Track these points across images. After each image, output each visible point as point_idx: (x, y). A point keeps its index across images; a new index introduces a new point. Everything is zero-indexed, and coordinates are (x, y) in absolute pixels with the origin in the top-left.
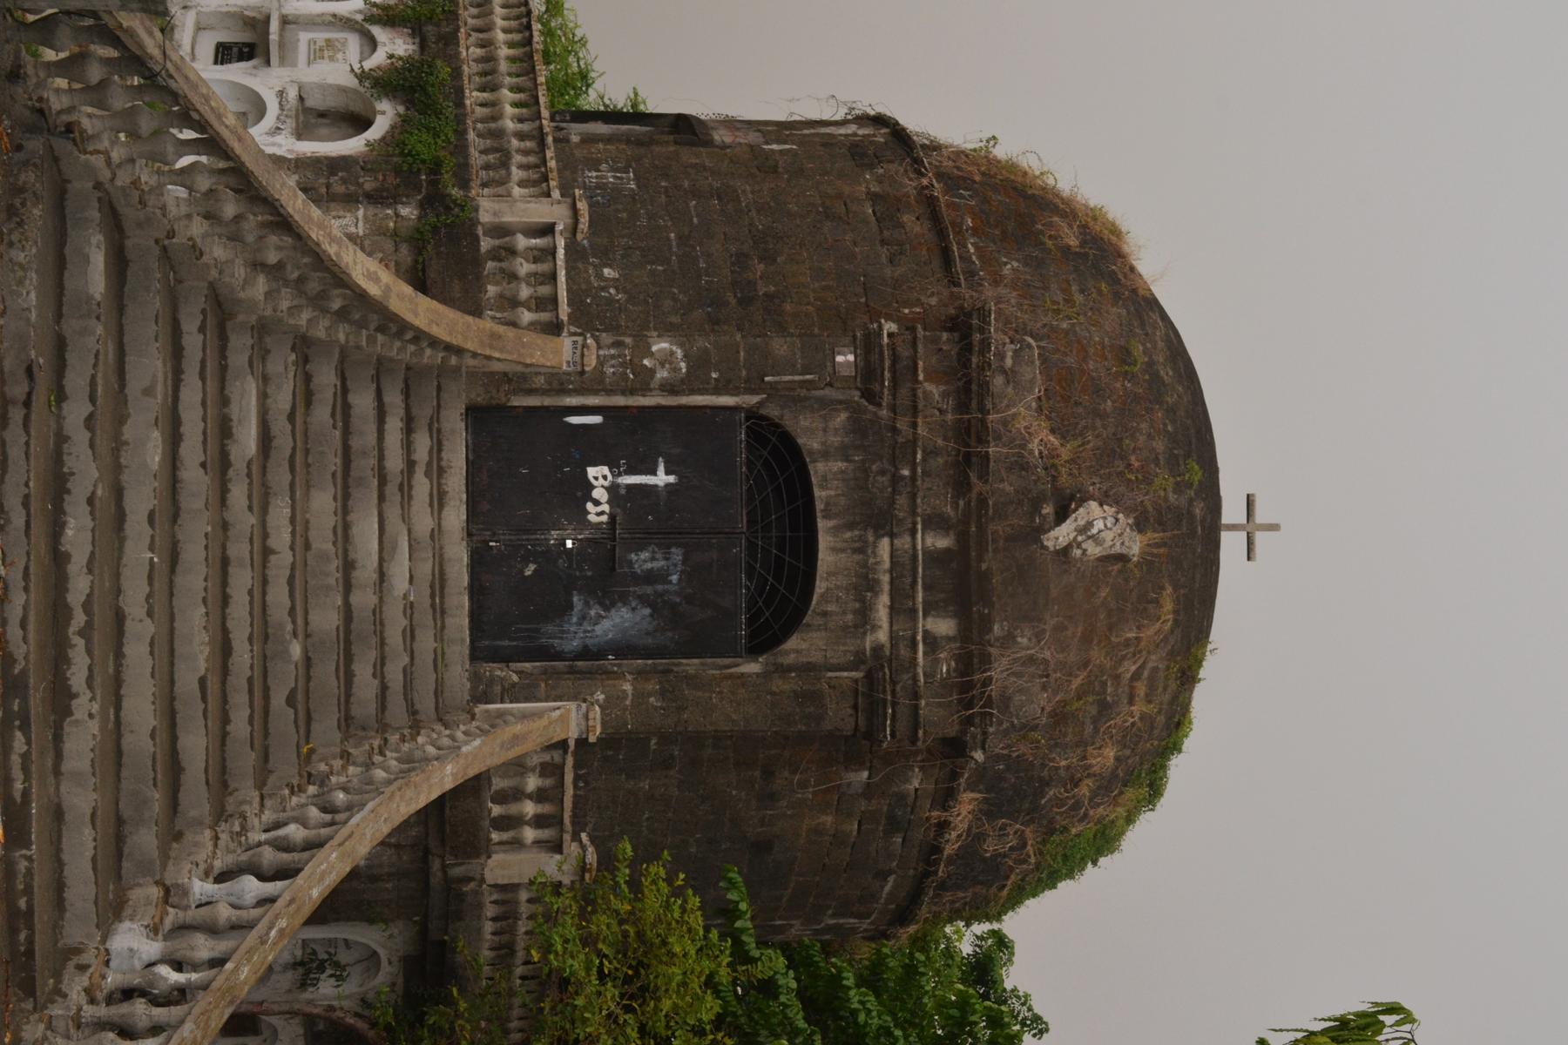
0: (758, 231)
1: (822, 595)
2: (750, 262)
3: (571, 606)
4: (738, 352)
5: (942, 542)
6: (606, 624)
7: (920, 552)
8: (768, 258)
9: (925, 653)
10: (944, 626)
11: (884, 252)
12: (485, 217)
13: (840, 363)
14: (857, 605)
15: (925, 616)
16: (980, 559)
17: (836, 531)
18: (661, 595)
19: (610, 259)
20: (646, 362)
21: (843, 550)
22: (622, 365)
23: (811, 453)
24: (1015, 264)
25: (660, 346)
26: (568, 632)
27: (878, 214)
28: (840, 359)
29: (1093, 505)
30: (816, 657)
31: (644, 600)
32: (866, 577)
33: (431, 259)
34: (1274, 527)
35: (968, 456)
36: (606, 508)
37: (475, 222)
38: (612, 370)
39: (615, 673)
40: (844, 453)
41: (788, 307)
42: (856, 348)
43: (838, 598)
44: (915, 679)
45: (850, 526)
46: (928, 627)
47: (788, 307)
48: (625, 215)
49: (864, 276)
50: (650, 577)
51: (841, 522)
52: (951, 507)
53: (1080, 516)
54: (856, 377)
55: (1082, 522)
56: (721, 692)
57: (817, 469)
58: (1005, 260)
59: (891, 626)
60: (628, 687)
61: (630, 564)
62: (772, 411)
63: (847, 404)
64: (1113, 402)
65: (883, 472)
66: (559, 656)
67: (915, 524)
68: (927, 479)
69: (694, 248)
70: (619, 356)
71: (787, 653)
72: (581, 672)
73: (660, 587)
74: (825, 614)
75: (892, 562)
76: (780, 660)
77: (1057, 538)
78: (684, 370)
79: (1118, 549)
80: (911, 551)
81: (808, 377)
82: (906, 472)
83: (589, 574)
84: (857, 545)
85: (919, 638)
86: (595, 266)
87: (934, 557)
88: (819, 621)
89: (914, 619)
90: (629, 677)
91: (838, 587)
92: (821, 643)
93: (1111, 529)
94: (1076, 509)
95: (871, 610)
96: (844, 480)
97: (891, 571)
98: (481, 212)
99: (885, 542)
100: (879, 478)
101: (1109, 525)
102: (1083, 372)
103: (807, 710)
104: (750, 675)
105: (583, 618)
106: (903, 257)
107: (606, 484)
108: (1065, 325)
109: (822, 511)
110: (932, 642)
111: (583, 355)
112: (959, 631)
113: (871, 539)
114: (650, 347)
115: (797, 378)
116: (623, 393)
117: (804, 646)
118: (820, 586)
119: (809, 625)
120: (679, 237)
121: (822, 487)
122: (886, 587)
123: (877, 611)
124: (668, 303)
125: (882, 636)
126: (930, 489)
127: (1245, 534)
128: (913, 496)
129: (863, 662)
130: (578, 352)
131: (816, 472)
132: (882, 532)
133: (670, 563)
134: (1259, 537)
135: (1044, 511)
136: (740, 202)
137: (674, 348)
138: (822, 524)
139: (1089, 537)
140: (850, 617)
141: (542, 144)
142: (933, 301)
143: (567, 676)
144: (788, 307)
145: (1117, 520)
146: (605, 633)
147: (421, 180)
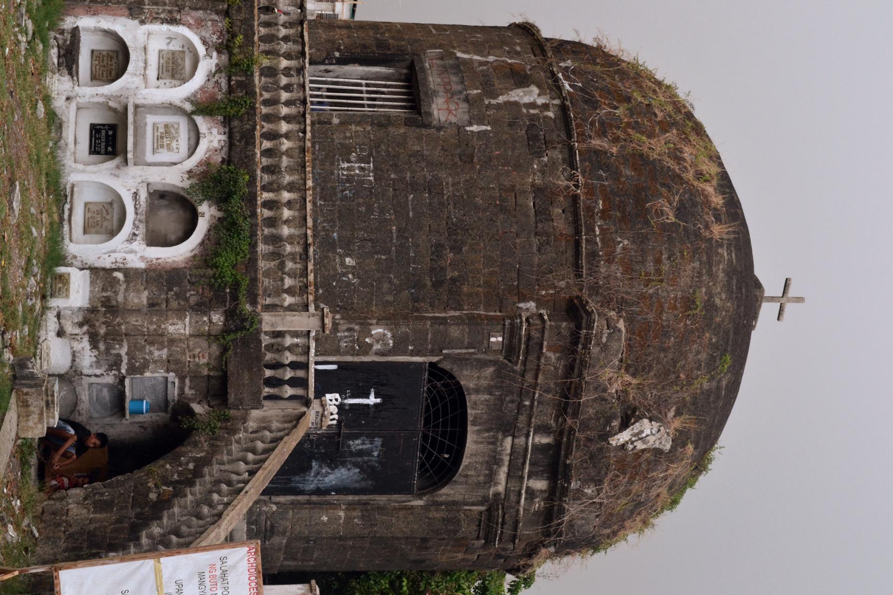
0: (452, 223)
1: (466, 466)
2: (444, 252)
3: (311, 468)
4: (427, 334)
5: (545, 440)
6: (331, 477)
7: (530, 447)
8: (456, 249)
9: (526, 499)
10: (540, 485)
11: (535, 241)
12: (266, 328)
13: (493, 342)
14: (487, 472)
15: (529, 478)
16: (567, 457)
17: (478, 432)
18: (366, 462)
19: (351, 250)
20: (367, 340)
21: (481, 443)
22: (353, 341)
23: (468, 389)
24: (626, 242)
25: (377, 331)
26: (308, 480)
27: (537, 208)
28: (493, 339)
29: (646, 421)
30: (458, 498)
31: (356, 465)
32: (494, 457)
33: (231, 357)
34: (800, 300)
35: (567, 404)
36: (336, 417)
37: (259, 331)
38: (345, 344)
39: (334, 504)
40: (489, 390)
41: (465, 289)
42: (504, 334)
43: (476, 468)
44: (518, 511)
45: (488, 430)
46: (530, 485)
47: (465, 289)
48: (363, 208)
49: (520, 264)
50: (360, 453)
51: (483, 427)
52: (554, 421)
53: (636, 427)
54: (502, 350)
55: (636, 431)
56: (398, 517)
57: (471, 399)
58: (619, 239)
59: (507, 483)
60: (342, 514)
61: (349, 446)
62: (446, 366)
63: (494, 363)
64: (676, 338)
65: (512, 402)
66: (301, 492)
67: (529, 432)
68: (540, 406)
69: (407, 238)
70: (350, 336)
71: (441, 495)
72: (315, 503)
73: (366, 458)
74: (466, 476)
75: (511, 450)
76: (436, 499)
77: (619, 440)
78: (391, 345)
79: (657, 445)
80: (524, 446)
81: (471, 351)
82: (527, 403)
83: (323, 451)
84: (492, 440)
85: (523, 492)
86: (340, 256)
87: (537, 448)
88: (463, 479)
89: (522, 482)
90: (343, 507)
91: (476, 462)
92: (463, 491)
93: (654, 435)
94: (634, 423)
95: (495, 474)
96: (487, 405)
97: (511, 455)
98: (263, 324)
99: (509, 439)
100: (510, 405)
101: (654, 432)
102: (656, 323)
103: (449, 528)
104: (417, 507)
105: (318, 473)
106: (548, 247)
107: (337, 403)
108: (651, 291)
109: (472, 421)
110: (531, 493)
111: (322, 420)
112: (549, 487)
113: (500, 437)
114: (370, 331)
115: (464, 351)
116: (352, 355)
117: (452, 492)
118: (465, 461)
119: (455, 482)
120: (399, 230)
121: (473, 408)
122: (507, 463)
123: (499, 475)
124: (386, 286)
125: (501, 488)
126: (541, 411)
127: (779, 304)
128: (530, 417)
129: (487, 501)
130: (319, 418)
131: (470, 400)
132: (507, 434)
133: (373, 446)
134: (788, 307)
135: (613, 424)
136: (443, 195)
137: (386, 332)
138: (470, 428)
139: (640, 439)
140: (482, 478)
141: (306, 247)
142: (562, 284)
143: (306, 506)
144: (465, 289)
145: (659, 430)
146: (331, 481)
147: (226, 293)
